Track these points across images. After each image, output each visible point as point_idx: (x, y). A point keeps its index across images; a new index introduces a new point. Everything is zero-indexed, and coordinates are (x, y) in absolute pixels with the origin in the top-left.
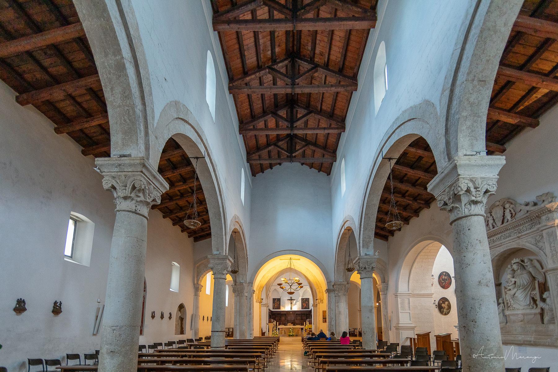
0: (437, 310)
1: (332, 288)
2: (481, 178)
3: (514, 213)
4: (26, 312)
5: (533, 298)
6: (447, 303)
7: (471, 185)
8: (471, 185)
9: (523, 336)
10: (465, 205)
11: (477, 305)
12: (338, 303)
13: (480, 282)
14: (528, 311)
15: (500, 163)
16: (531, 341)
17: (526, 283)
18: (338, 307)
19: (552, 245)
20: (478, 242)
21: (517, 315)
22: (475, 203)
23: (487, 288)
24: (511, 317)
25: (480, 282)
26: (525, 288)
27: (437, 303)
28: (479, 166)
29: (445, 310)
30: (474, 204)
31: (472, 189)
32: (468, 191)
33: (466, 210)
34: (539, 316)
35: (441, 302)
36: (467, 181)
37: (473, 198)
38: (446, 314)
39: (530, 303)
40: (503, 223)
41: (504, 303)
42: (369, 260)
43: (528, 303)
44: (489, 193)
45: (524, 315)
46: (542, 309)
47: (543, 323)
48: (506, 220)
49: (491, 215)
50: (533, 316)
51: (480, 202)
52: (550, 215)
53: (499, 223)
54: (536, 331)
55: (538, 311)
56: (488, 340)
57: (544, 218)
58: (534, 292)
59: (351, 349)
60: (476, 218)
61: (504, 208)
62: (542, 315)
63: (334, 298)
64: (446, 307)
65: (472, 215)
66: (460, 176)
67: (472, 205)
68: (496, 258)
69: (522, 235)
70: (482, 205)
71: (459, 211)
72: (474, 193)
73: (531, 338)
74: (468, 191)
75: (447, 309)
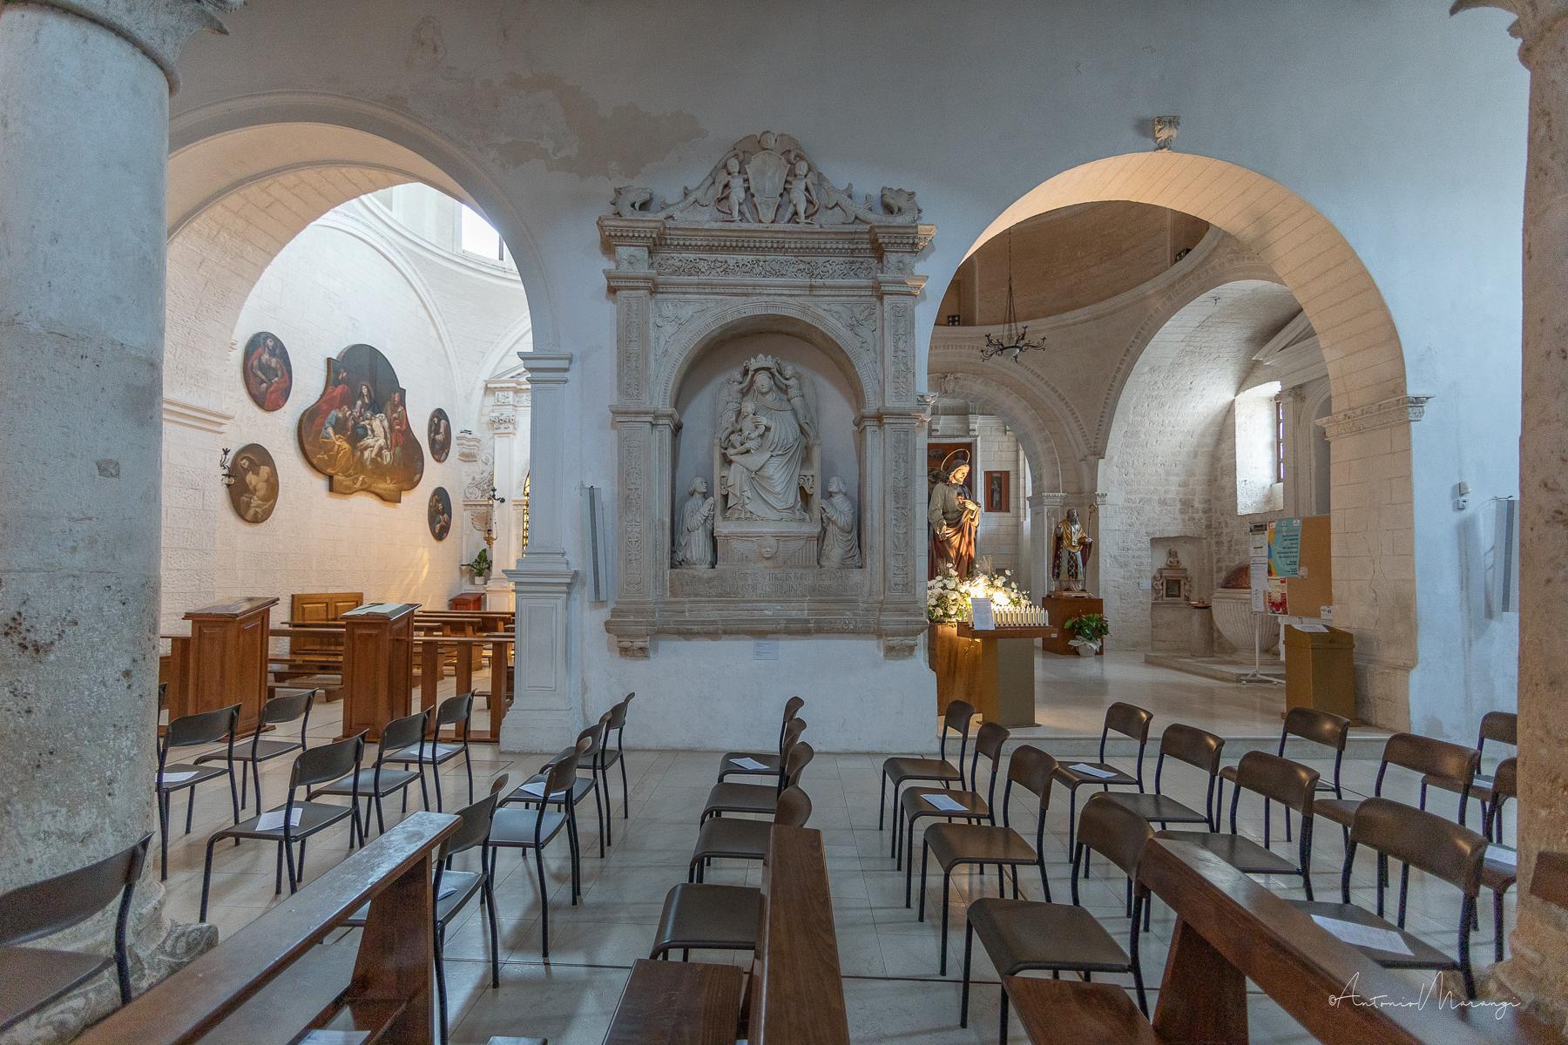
4: (298, 592)
5: (802, 489)
6: (265, 470)
14: (794, 528)
21: (760, 536)
24: (735, 544)
29: (255, 501)
35: (245, 463)
38: (256, 520)
43: (791, 501)
45: (778, 537)
52: (907, 258)
64: (262, 488)
69: (824, 287)
73: (799, 610)
75: (265, 499)
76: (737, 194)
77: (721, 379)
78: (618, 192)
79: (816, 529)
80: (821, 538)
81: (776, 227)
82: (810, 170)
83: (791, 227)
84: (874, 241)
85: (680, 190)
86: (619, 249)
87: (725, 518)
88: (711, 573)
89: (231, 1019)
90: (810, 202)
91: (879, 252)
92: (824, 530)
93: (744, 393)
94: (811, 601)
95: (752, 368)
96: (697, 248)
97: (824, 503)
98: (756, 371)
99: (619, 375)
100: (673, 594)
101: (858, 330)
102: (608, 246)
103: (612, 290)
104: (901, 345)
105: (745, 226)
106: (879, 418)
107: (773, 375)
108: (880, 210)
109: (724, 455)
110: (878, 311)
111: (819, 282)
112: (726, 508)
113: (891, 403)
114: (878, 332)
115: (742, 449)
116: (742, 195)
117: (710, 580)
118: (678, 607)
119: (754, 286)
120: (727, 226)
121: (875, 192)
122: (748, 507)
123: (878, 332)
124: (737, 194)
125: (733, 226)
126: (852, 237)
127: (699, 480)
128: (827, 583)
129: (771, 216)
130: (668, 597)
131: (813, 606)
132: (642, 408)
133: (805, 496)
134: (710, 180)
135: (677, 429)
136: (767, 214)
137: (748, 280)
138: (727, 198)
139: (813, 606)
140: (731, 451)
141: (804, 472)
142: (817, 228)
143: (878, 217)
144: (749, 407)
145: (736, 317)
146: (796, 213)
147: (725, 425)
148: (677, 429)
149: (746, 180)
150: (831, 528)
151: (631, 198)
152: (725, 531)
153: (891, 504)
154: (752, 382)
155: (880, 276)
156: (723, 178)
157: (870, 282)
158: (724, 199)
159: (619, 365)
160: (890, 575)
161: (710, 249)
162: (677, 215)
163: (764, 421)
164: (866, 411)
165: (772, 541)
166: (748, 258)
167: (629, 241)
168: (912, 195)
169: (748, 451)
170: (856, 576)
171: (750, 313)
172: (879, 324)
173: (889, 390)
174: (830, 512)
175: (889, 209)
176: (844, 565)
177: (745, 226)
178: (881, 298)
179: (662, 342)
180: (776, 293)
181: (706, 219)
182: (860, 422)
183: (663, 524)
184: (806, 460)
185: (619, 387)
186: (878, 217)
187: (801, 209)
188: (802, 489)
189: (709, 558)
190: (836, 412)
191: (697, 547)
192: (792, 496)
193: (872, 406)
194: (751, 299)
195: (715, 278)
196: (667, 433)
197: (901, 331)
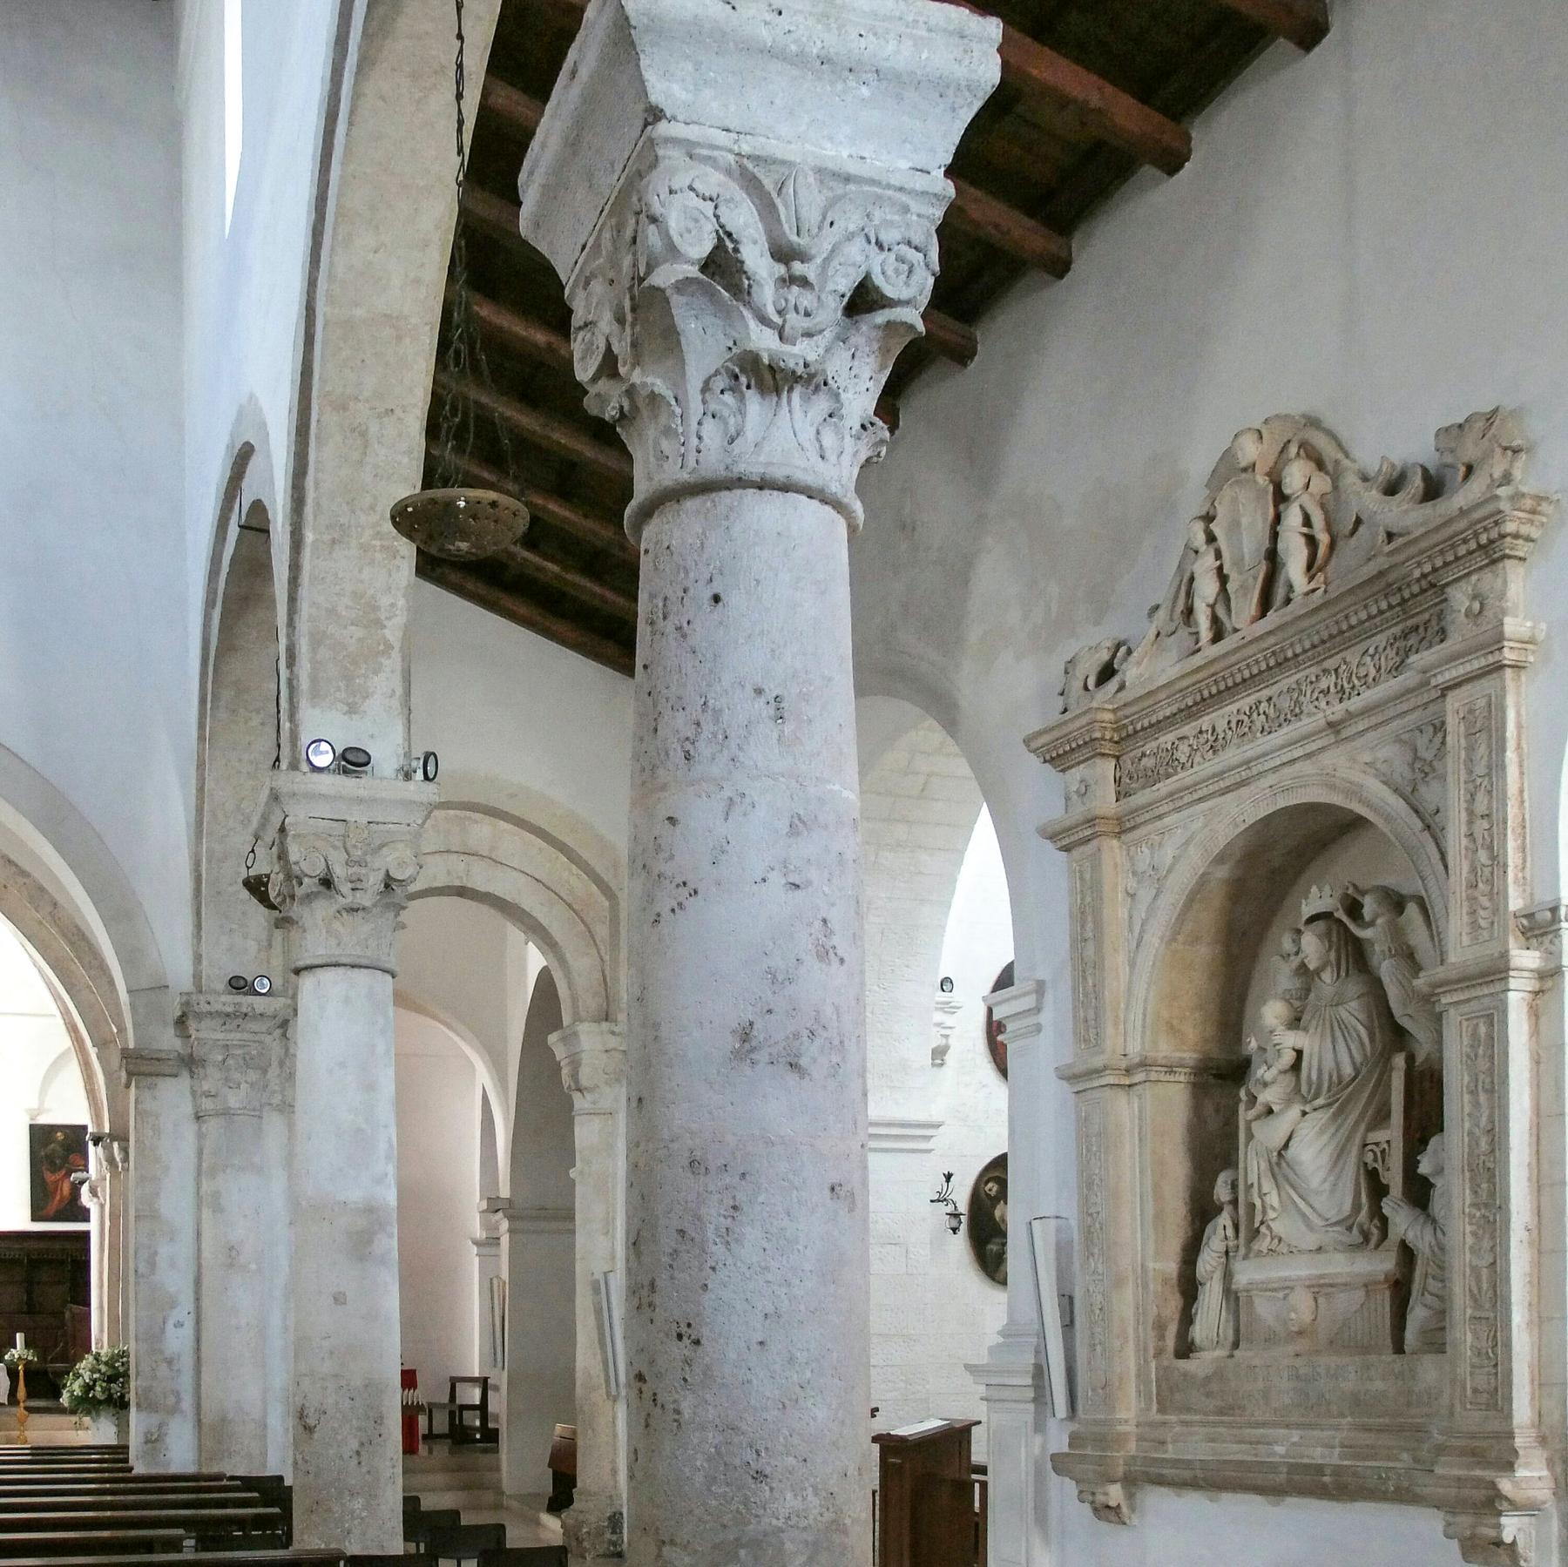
0: (959, 1245)
1: (168, 1041)
2: (827, 175)
3: (1323, 538)
7: (744, 219)
8: (744, 219)
9: (1295, 1436)
10: (706, 388)
11: (714, 1214)
12: (213, 1173)
13: (745, 1034)
15: (960, 72)
16: (1319, 1469)
17: (1348, 1070)
18: (218, 1209)
19: (1481, 797)
20: (760, 707)
22: (767, 378)
23: (792, 1078)
25: (745, 1034)
26: (1339, 1096)
27: (961, 1198)
28: (799, 60)
30: (763, 390)
31: (756, 260)
32: (722, 265)
33: (710, 427)
34: (1384, 1300)
36: (713, 181)
37: (763, 341)
39: (1356, 1207)
40: (1265, 604)
41: (1234, 1202)
42: (358, 816)
44: (881, 317)
45: (1320, 1288)
46: (1407, 1254)
47: (1399, 1348)
48: (1280, 593)
49: (1211, 538)
50: (1361, 1293)
51: (810, 380)
53: (1245, 605)
54: (1356, 1402)
55: (1383, 1264)
56: (760, 1476)
57: (1460, 598)
58: (1380, 1136)
59: (174, 1545)
60: (765, 510)
61: (1281, 497)
62: (1400, 1290)
63: (189, 1131)
65: (740, 483)
66: (663, 128)
67: (752, 397)
68: (1222, 872)
69: (1350, 716)
70: (822, 404)
71: (668, 432)
72: (767, 295)
73: (1322, 1448)
74: (722, 265)
104: (1481, 806)
128: (1379, 1385)
130: (1154, 1415)
145: (1233, 833)
149: (1218, 555)
189: (1231, 1338)
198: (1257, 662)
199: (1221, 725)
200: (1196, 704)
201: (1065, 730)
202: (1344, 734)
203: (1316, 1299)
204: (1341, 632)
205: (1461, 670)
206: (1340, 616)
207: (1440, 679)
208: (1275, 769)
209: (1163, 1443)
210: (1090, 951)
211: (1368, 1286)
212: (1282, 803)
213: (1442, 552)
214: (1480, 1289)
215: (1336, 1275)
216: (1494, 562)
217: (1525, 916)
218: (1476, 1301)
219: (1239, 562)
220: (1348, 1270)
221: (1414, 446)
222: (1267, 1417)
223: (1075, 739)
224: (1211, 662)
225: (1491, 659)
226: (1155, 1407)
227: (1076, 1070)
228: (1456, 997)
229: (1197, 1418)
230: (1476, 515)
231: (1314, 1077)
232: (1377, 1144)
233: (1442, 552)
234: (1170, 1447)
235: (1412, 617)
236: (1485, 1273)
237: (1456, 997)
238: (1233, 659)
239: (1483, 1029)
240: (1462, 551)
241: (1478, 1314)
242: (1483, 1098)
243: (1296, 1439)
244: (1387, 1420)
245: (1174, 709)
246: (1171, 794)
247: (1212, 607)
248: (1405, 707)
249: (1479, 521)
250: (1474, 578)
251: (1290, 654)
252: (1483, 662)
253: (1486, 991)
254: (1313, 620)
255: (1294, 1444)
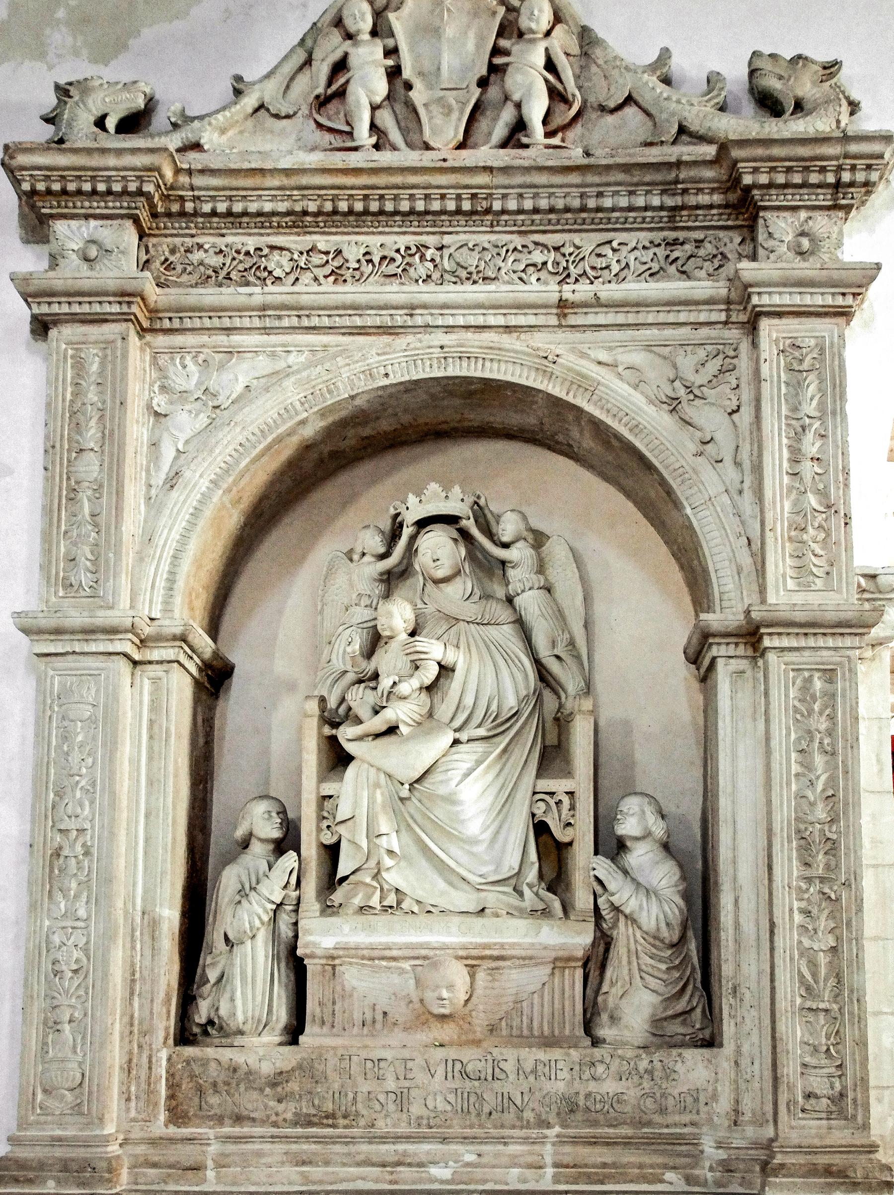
24: (352, 977)
43: (512, 861)
52: (821, 223)
69: (597, 303)
76: (369, 83)
77: (326, 550)
78: (63, 92)
79: (580, 938)
80: (596, 961)
81: (467, 157)
82: (557, 18)
83: (506, 157)
84: (733, 182)
85: (226, 87)
86: (60, 227)
87: (328, 909)
88: (288, 1058)
89: (600, 796)
90: (557, 95)
91: (744, 210)
92: (604, 942)
93: (391, 581)
94: (561, 1140)
95: (410, 517)
96: (263, 219)
97: (603, 867)
98: (423, 524)
99: (47, 538)
100: (177, 1116)
101: (689, 411)
102: (36, 226)
103: (41, 327)
104: (811, 446)
105: (385, 158)
106: (751, 636)
107: (465, 535)
108: (749, 107)
109: (333, 741)
110: (744, 363)
111: (583, 291)
112: (331, 880)
113: (784, 595)
114: (745, 417)
115: (378, 723)
116: (381, 87)
117: (278, 1080)
118: (185, 1154)
119: (411, 308)
120: (338, 160)
121: (735, 73)
122: (393, 878)
123: (745, 417)
124: (369, 83)
125: (354, 160)
126: (669, 176)
127: (261, 808)
128: (610, 1087)
129: (455, 130)
130: (160, 1126)
131: (569, 1153)
132: (104, 618)
133: (551, 850)
134: (301, 56)
135: (215, 679)
136: (443, 130)
137: (394, 292)
138: (341, 93)
139: (569, 1153)
140: (346, 733)
141: (545, 784)
142: (576, 155)
143: (744, 123)
144: (398, 615)
145: (364, 385)
146: (520, 126)
147: (338, 664)
148: (215, 679)
149: (391, 52)
150: (623, 933)
151: (95, 105)
152: (328, 942)
153: (788, 867)
154: (411, 551)
155: (748, 269)
156: (331, 48)
157: (718, 288)
158: (333, 96)
159: (48, 511)
160: (790, 1069)
161: (298, 220)
162: (209, 138)
163: (434, 650)
164: (713, 620)
165: (458, 974)
166: (397, 240)
167: (84, 205)
168: (831, 68)
169: (392, 730)
170: (693, 1068)
171: (399, 376)
172: (746, 394)
173: (779, 563)
174: (621, 892)
175: (769, 104)
176: (661, 1037)
177: (385, 158)
178: (752, 327)
179: (168, 453)
180: (475, 318)
181: (290, 148)
182: (699, 655)
183: (153, 925)
184: (552, 756)
185: (45, 568)
186: (744, 123)
187: (537, 109)
188: (541, 829)
189: (282, 1015)
190: (636, 626)
191: (247, 986)
192: (515, 848)
193: (725, 616)
194: (401, 342)
195: (307, 290)
196: (180, 689)
197: (810, 408)
198: (412, 197)
199: (353, 254)
200: (319, 213)
201: (96, 161)
202: (572, 320)
203: (472, 976)
204: (583, 209)
205: (787, 300)
206: (593, 190)
207: (766, 300)
208: (449, 329)
209: (197, 1168)
210: (90, 468)
211: (560, 963)
212: (455, 370)
213: (789, 170)
214: (814, 975)
215: (513, 945)
216: (836, 207)
217: (865, 576)
218: (808, 989)
219: (431, 76)
220: (528, 940)
221: (652, 56)
222: (403, 1129)
223: (108, 179)
224: (403, 170)
225: (840, 301)
226: (162, 1116)
227: (44, 623)
228: (785, 642)
229: (258, 1130)
230: (854, 148)
231: (469, 701)
232: (552, 794)
233: (789, 170)
234: (210, 1174)
235: (675, 229)
236: (823, 959)
237: (785, 642)
238: (398, 179)
239: (818, 684)
240: (814, 178)
241: (808, 1004)
242: (819, 760)
243: (470, 1158)
244: (629, 1131)
245: (282, 207)
246: (264, 308)
247: (374, 108)
248: (671, 318)
249: (855, 157)
250: (803, 214)
251: (497, 206)
252: (829, 300)
253: (830, 642)
254: (558, 179)
255: (468, 1165)
